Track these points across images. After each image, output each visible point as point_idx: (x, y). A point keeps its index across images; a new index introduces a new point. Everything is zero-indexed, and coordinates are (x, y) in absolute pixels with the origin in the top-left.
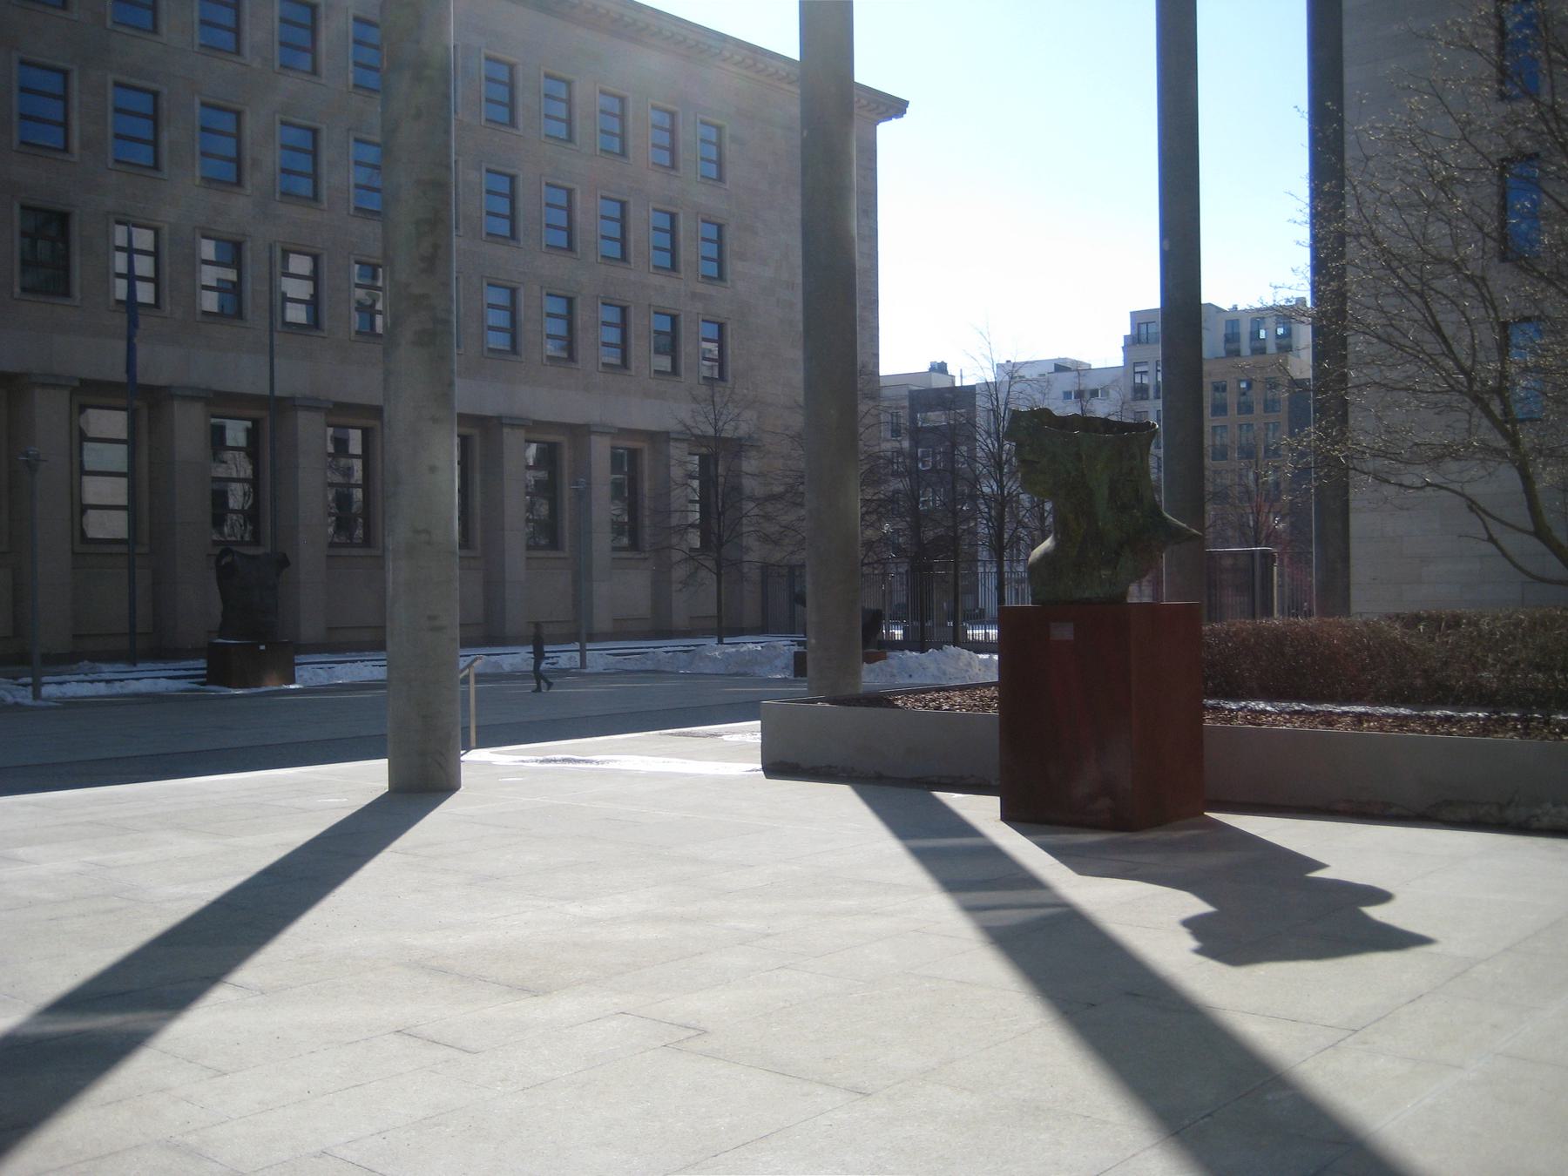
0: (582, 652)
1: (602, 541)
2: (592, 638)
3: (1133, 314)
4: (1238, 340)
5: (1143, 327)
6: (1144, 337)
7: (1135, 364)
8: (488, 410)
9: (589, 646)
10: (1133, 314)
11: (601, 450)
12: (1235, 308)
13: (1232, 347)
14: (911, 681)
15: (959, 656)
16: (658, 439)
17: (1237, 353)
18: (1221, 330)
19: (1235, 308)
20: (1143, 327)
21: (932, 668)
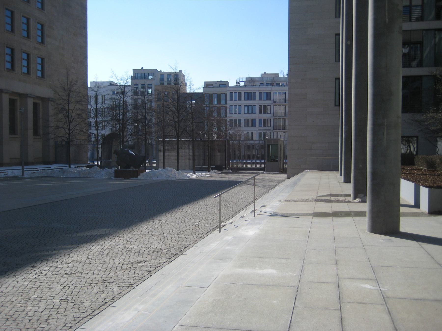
0: (23, 169)
1: (31, 132)
2: (27, 164)
3: (205, 82)
4: (164, 81)
5: (137, 74)
6: (137, 77)
7: (135, 85)
8: (20, 90)
9: (25, 167)
10: (205, 82)
11: (30, 102)
12: (161, 71)
13: (162, 82)
14: (158, 179)
15: (171, 171)
16: (45, 100)
17: (163, 84)
18: (159, 77)
19: (161, 71)
20: (137, 74)
21: (164, 175)
